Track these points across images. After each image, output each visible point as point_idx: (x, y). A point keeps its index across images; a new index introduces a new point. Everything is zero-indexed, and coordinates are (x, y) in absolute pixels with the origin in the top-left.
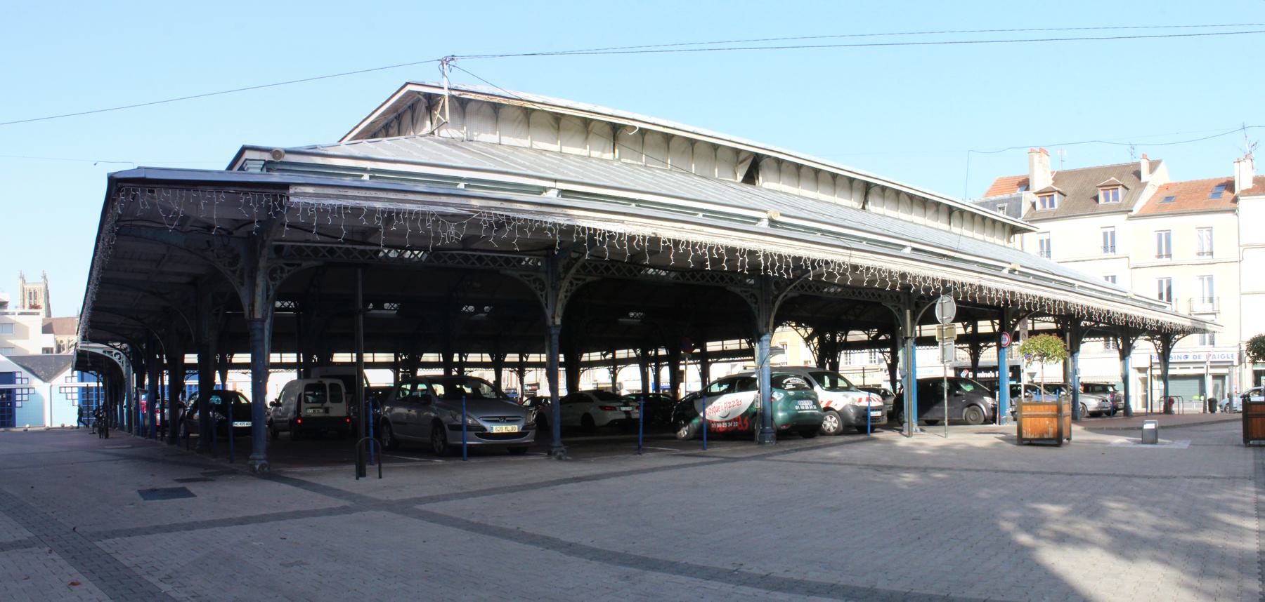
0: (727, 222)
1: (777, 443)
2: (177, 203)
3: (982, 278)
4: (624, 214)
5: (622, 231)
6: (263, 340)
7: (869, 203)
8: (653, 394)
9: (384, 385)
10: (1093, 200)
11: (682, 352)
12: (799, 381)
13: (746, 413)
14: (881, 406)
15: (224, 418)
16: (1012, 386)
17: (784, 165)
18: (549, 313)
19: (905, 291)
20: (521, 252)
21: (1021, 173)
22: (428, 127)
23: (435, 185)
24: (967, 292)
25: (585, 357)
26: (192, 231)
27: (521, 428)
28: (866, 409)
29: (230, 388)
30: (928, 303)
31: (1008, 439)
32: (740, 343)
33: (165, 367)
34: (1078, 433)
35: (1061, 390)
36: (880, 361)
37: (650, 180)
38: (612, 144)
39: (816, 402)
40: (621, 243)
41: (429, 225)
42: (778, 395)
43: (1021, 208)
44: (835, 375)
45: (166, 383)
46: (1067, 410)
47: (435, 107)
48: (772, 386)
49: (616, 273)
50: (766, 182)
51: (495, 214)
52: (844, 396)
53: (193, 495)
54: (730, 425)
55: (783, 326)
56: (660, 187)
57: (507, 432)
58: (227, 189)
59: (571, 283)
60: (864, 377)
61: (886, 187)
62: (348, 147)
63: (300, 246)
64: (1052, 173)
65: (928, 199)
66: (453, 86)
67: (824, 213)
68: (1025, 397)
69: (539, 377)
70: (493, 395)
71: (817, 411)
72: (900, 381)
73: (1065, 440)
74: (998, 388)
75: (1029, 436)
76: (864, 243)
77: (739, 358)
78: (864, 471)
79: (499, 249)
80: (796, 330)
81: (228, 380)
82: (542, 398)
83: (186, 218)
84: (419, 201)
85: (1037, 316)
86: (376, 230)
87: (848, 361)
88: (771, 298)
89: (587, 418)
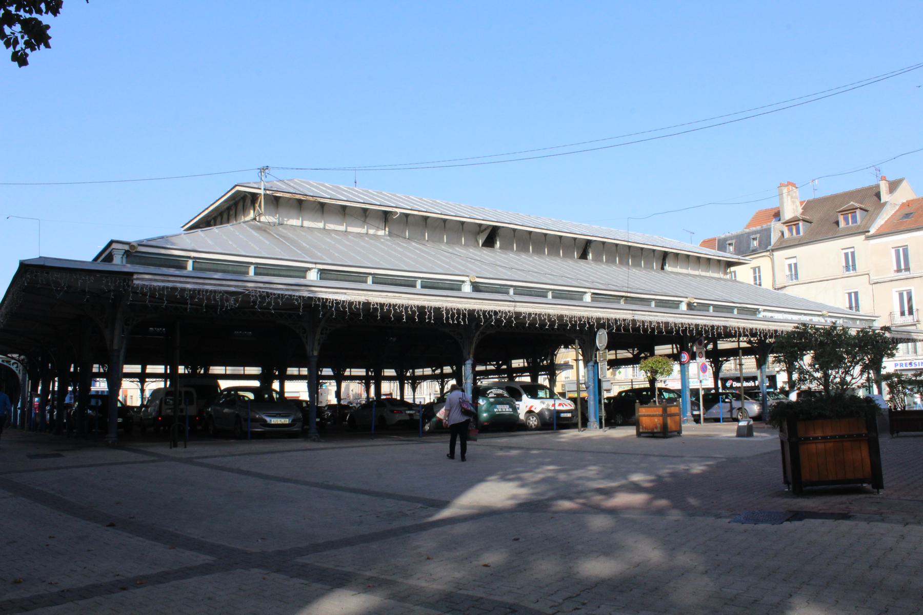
10: (835, 224)
12: (500, 391)
18: (308, 348)
21: (772, 204)
22: (252, 214)
40: (344, 307)
51: (259, 291)
52: (541, 402)
53: (63, 456)
64: (801, 203)
89: (382, 420)
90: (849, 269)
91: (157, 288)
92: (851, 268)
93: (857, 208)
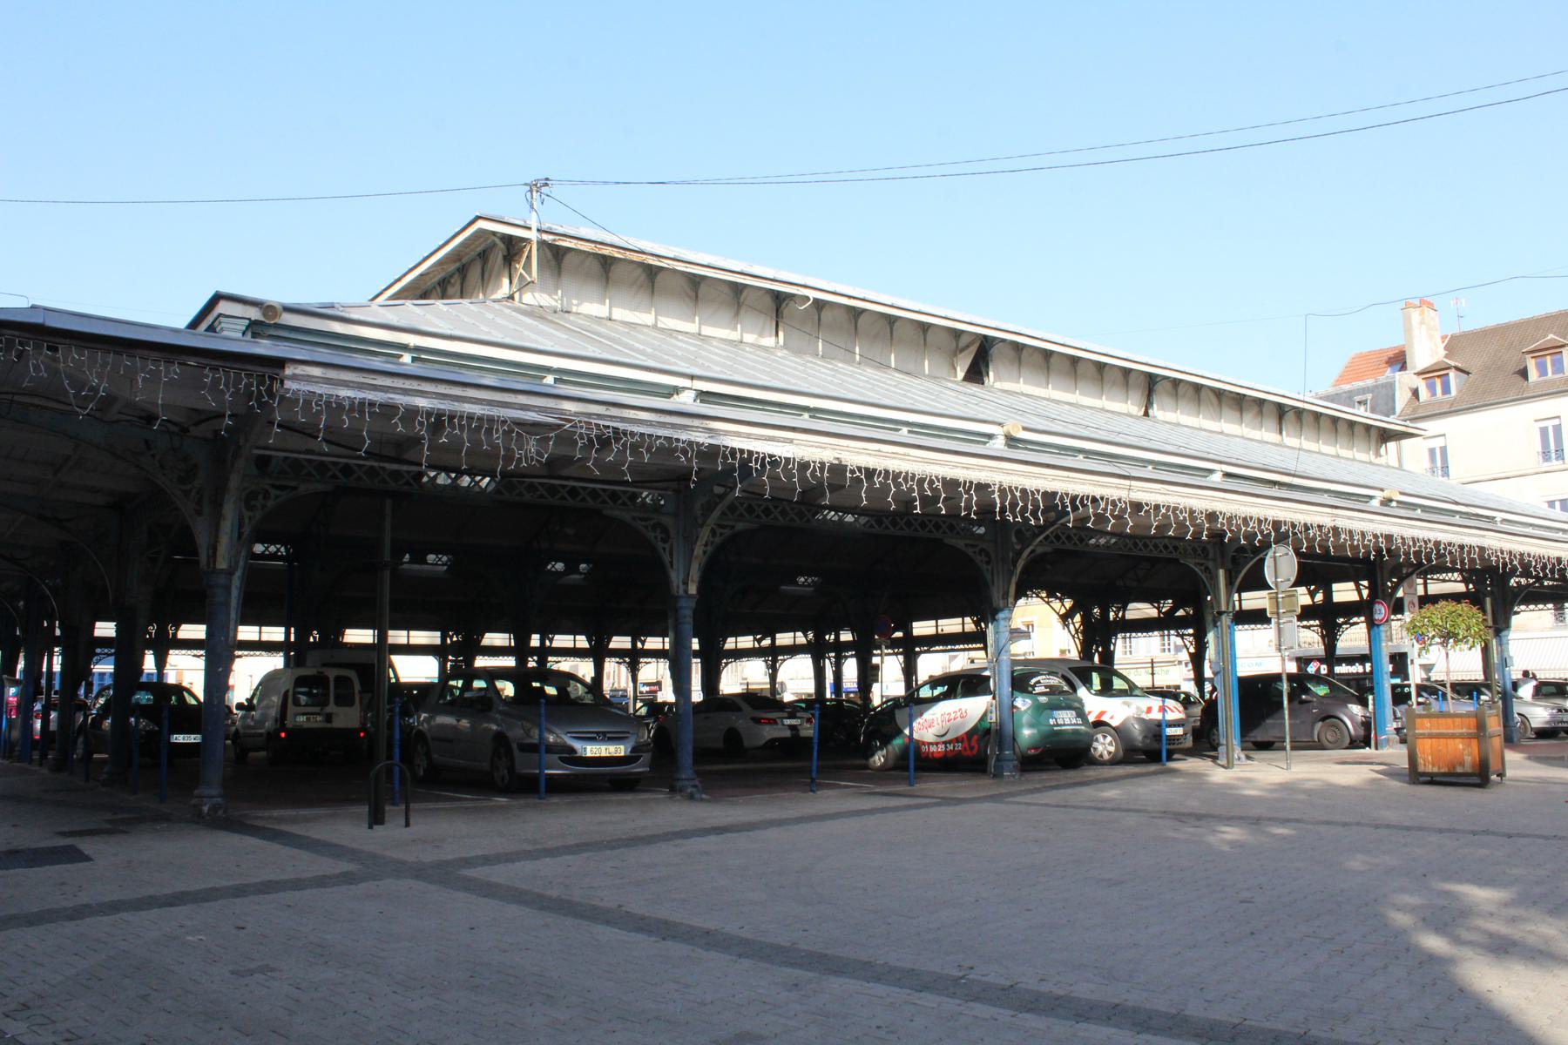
0: (944, 440)
1: (1021, 775)
2: (98, 375)
3: (1337, 516)
4: (793, 429)
5: (789, 455)
6: (227, 604)
7: (1155, 406)
8: (831, 700)
9: (423, 680)
11: (876, 637)
12: (1055, 681)
13: (974, 730)
14: (1182, 719)
15: (156, 728)
16: (1394, 687)
17: (1025, 353)
18: (675, 577)
19: (1215, 540)
20: (635, 483)
21: (1392, 342)
22: (504, 288)
23: (511, 377)
24: (1314, 539)
25: (730, 644)
26: (118, 421)
27: (629, 750)
28: (1159, 725)
29: (171, 679)
30: (1252, 558)
31: (1392, 773)
32: (963, 624)
33: (58, 641)
34: (1517, 765)
35: (1480, 693)
36: (1178, 649)
37: (830, 378)
38: (774, 323)
39: (1081, 714)
41: (498, 438)
42: (1023, 703)
43: (1394, 401)
44: (1108, 670)
45: (57, 668)
46: (1494, 725)
47: (517, 258)
48: (1013, 689)
49: (780, 518)
50: (998, 380)
52: (1125, 703)
53: (87, 859)
54: (951, 747)
55: (1027, 596)
56: (844, 389)
57: (608, 755)
58: (183, 358)
59: (713, 532)
60: (1153, 674)
61: (1181, 381)
62: (381, 310)
63: (296, 459)
64: (1443, 338)
65: (1245, 395)
66: (544, 227)
67: (1087, 423)
68: (1419, 704)
69: (660, 672)
70: (589, 699)
71: (1083, 728)
72: (1211, 680)
73: (1494, 777)
74: (1371, 690)
75: (1430, 769)
76: (1150, 467)
77: (962, 646)
78: (1160, 821)
79: (601, 478)
80: (1048, 603)
81: (168, 666)
82: (664, 704)
83: (110, 400)
84: (484, 400)
85: (1432, 573)
86: (416, 441)
87: (1128, 649)
88: (1011, 554)
89: (733, 736)
90: (1550, 457)
91: (347, 403)
92: (1553, 455)
93: (1448, 368)
